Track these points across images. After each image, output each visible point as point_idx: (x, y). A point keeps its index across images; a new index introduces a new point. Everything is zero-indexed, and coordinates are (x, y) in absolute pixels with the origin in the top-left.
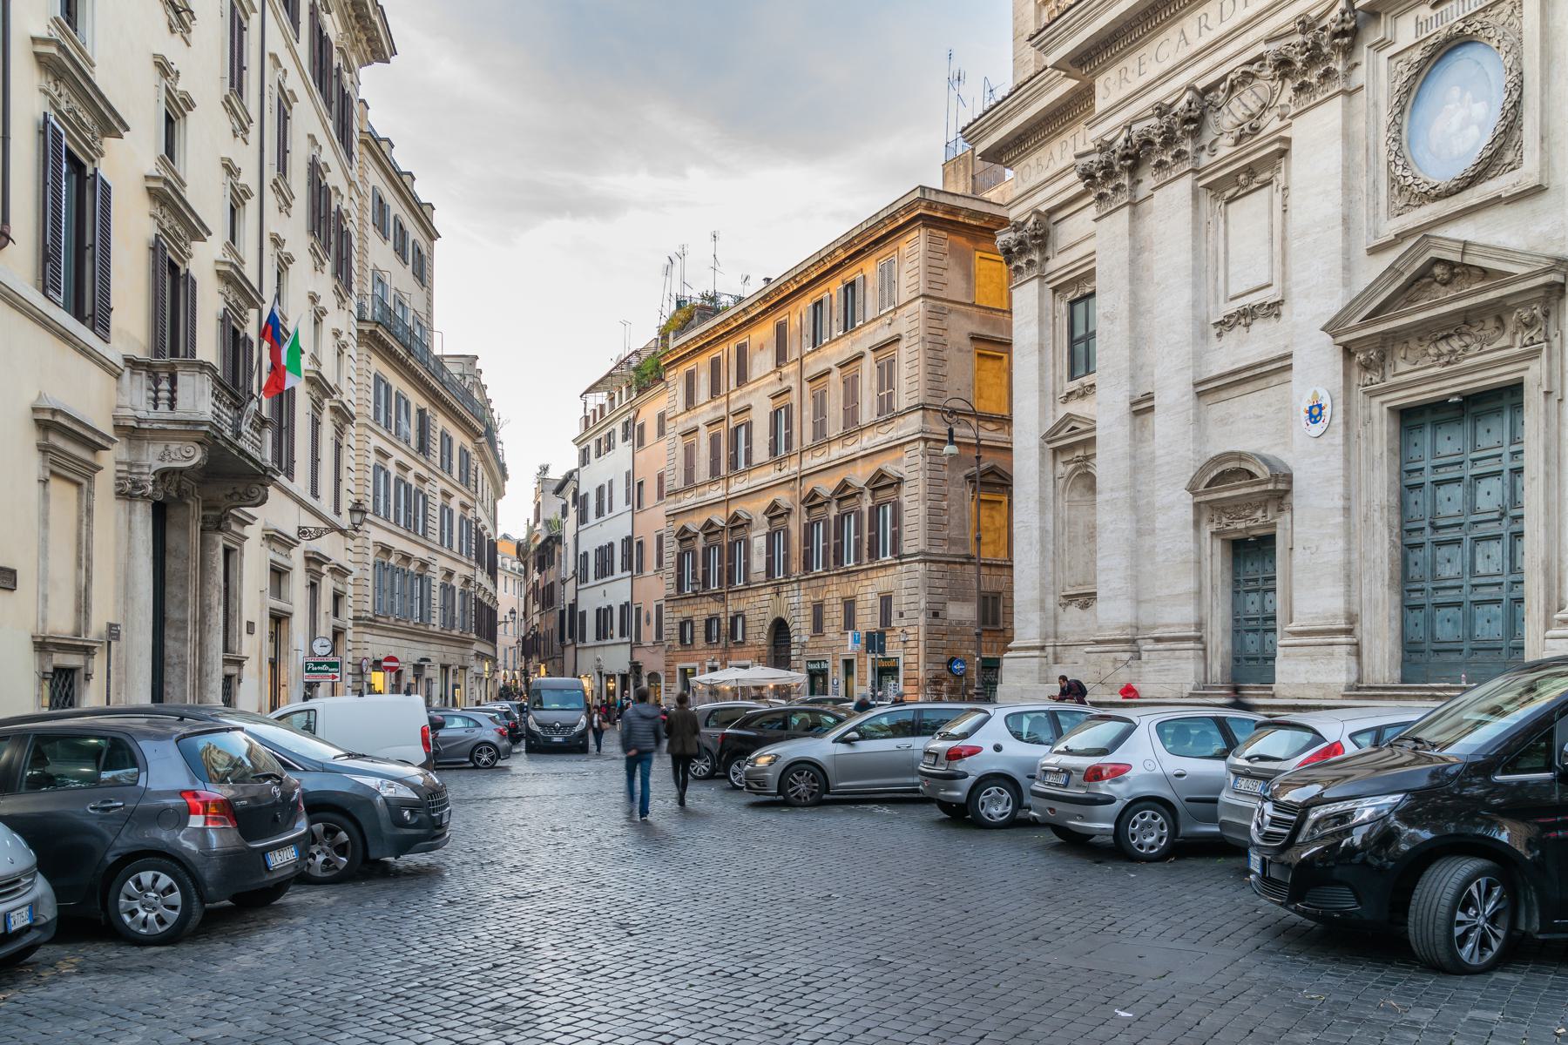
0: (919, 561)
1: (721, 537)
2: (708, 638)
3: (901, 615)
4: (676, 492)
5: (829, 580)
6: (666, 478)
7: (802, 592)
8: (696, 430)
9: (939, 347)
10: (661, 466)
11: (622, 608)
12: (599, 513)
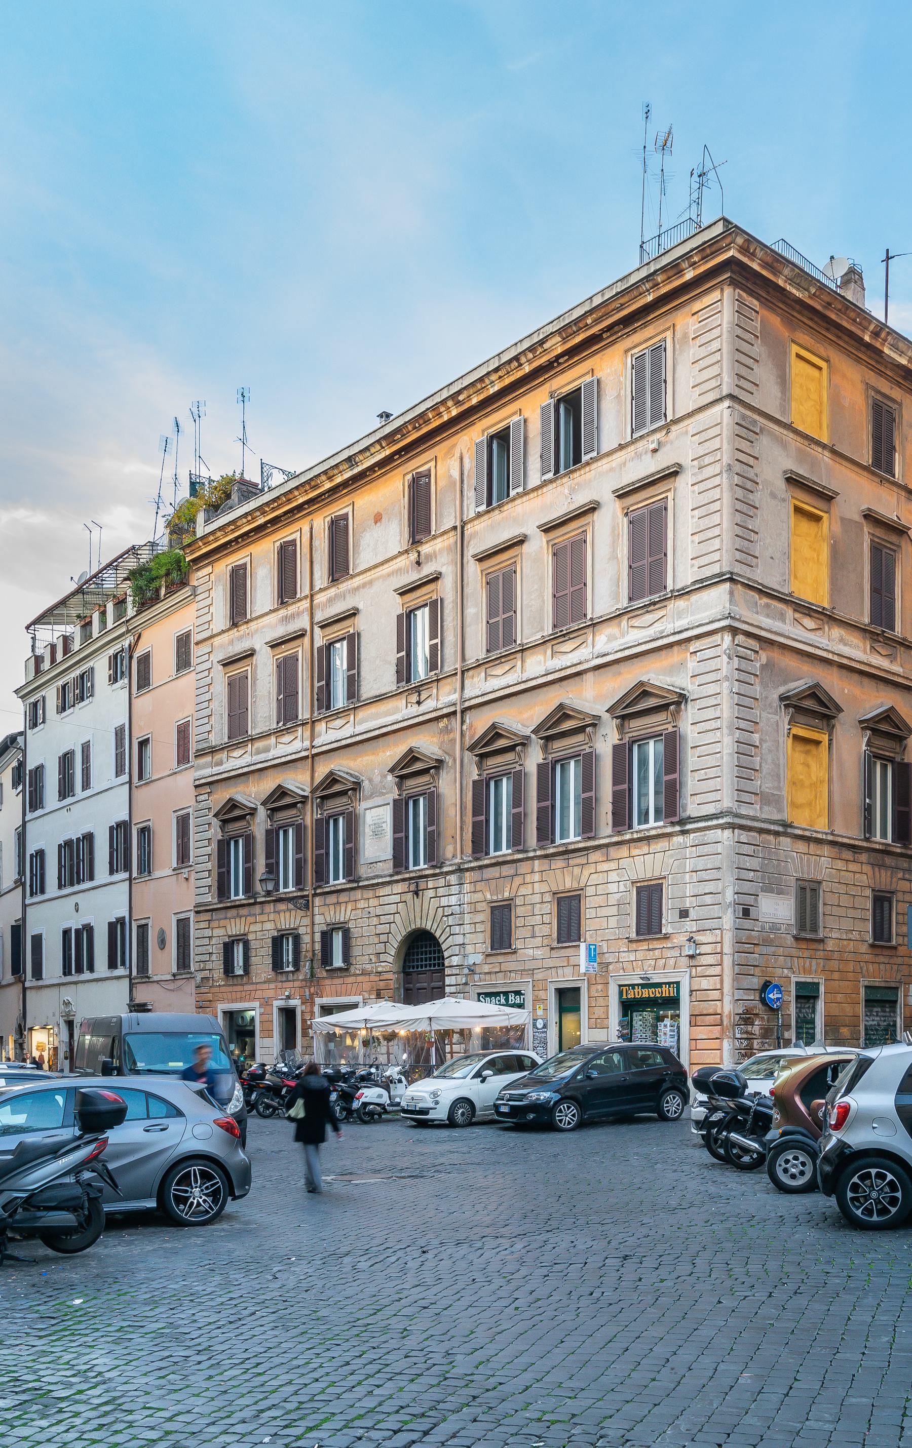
0: (722, 827)
1: (302, 813)
2: (277, 964)
3: (684, 914)
4: (213, 751)
5: (524, 868)
6: (193, 731)
7: (467, 887)
8: (250, 654)
9: (749, 485)
10: (186, 712)
11: (112, 927)
12: (66, 789)
